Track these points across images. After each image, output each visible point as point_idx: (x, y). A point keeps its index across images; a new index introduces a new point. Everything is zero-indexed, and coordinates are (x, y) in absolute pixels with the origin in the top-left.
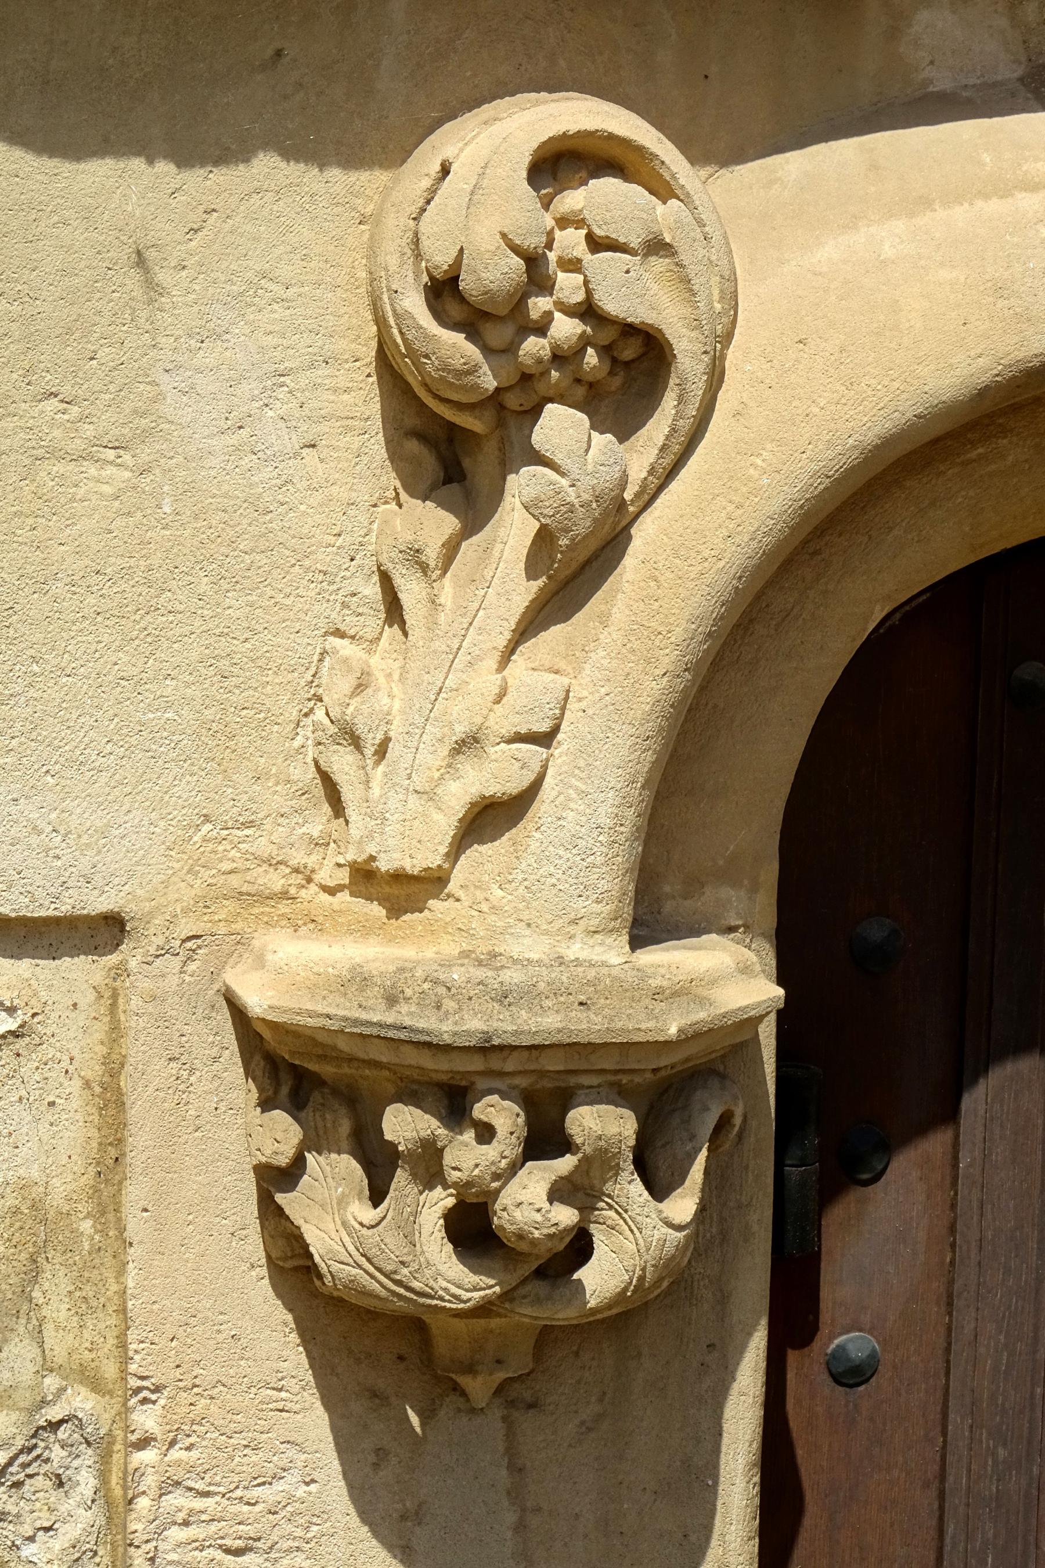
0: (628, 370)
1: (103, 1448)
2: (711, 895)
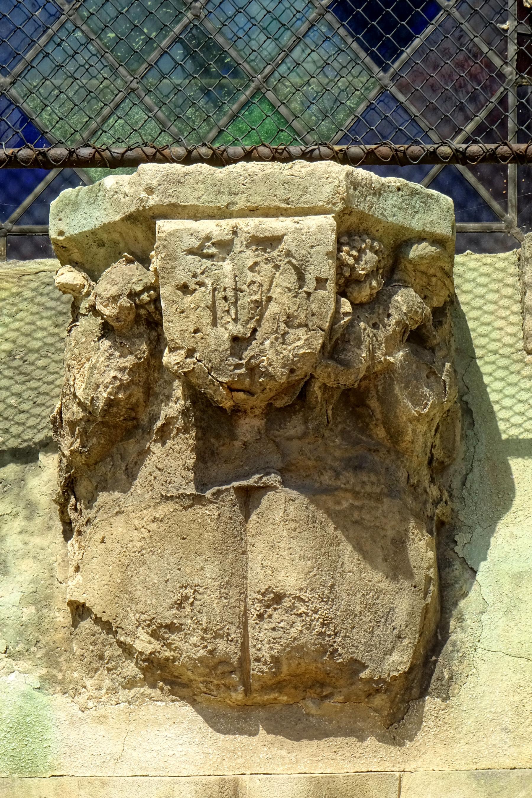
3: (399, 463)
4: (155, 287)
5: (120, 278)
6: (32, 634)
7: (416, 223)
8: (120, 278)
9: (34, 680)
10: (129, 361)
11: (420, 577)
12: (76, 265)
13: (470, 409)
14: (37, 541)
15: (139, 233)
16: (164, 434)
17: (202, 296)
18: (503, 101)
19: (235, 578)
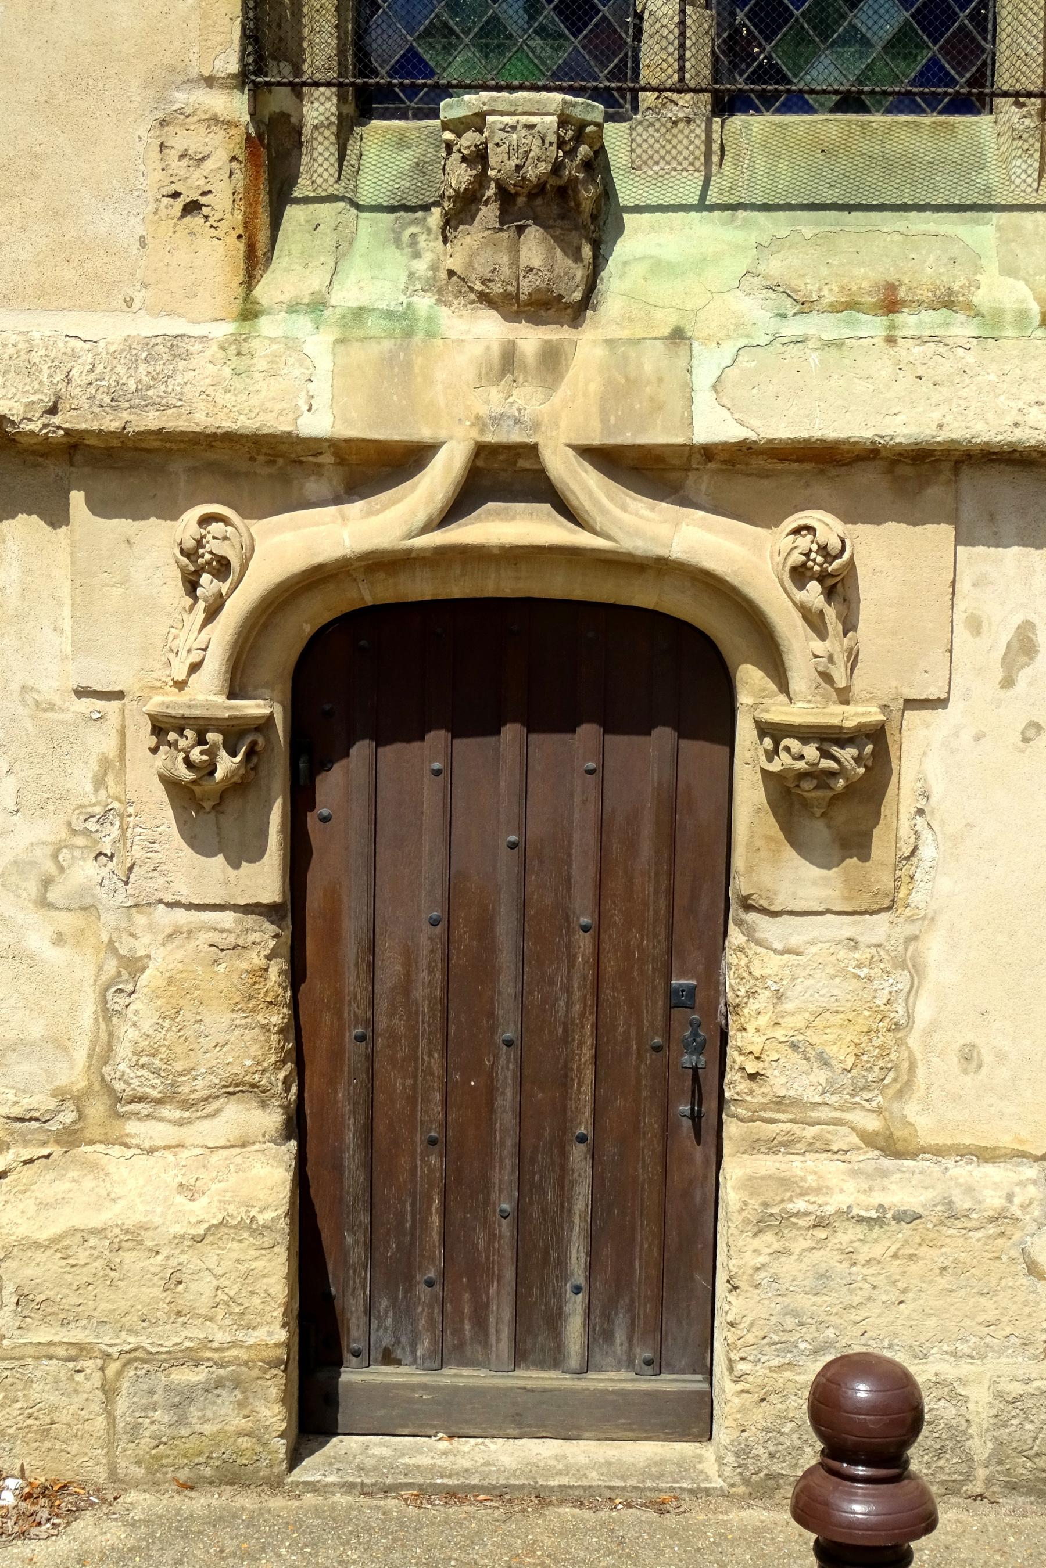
0: (222, 567)
1: (121, 816)
2: (260, 691)
3: (1015, 1210)
4: (486, 143)
5: (469, 139)
6: (432, 282)
7: (589, 118)
8: (469, 139)
9: (433, 300)
10: (474, 172)
11: (586, 262)
12: (452, 131)
13: (608, 192)
14: (432, 244)
15: (478, 120)
16: (487, 203)
17: (505, 148)
18: (626, 55)
19: (515, 262)
